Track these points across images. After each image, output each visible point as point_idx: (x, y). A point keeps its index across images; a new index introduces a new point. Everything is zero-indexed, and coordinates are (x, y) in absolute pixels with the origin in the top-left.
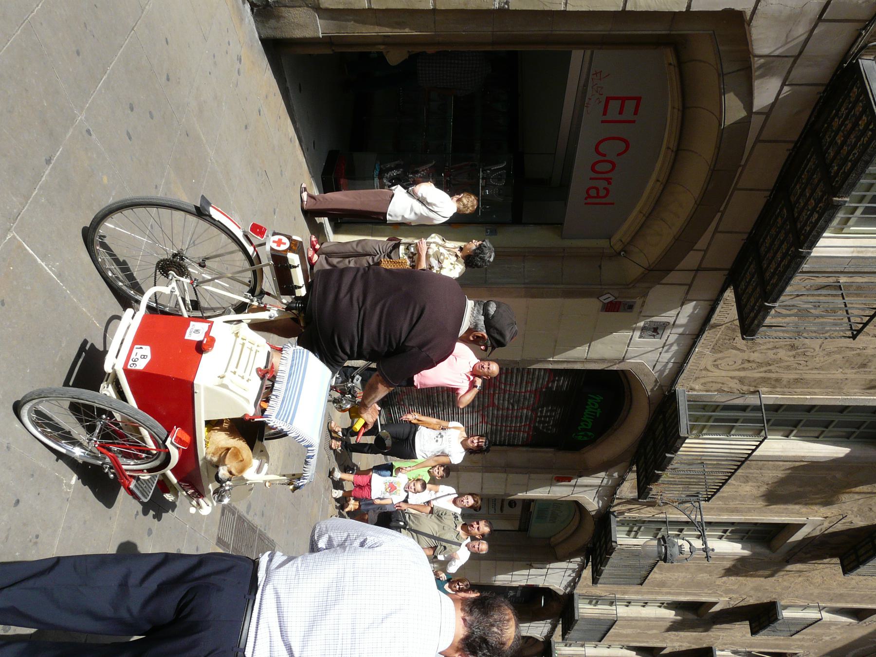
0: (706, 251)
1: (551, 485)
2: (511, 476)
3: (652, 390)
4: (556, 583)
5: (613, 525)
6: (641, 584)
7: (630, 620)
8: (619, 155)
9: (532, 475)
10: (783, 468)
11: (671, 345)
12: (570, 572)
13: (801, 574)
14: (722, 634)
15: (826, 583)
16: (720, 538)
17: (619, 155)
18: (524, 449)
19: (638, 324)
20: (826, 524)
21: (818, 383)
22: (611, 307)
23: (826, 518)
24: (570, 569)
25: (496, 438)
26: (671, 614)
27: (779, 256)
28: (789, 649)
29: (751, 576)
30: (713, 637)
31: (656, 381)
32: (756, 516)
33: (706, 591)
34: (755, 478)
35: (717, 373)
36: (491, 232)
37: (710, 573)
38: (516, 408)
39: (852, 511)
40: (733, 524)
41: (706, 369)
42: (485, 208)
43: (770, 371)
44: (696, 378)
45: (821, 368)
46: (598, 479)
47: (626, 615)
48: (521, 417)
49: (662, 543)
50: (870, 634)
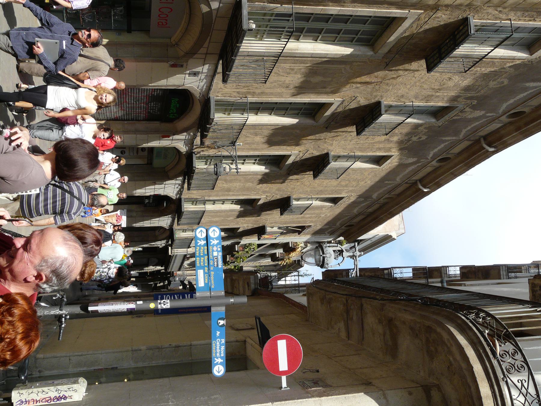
0: (208, 48)
1: (160, 140)
2: (138, 136)
3: (199, 97)
4: (170, 193)
5: (194, 159)
6: (213, 189)
7: (216, 212)
8: (169, 12)
10: (271, 129)
11: (203, 80)
12: (177, 185)
13: (298, 180)
14: (269, 217)
15: (311, 184)
16: (254, 163)
17: (169, 12)
18: (144, 122)
19: (187, 72)
20: (301, 155)
21: (272, 94)
22: (173, 66)
23: (300, 151)
24: (177, 184)
25: (129, 117)
26: (238, 207)
28: (306, 223)
29: (274, 183)
30: (264, 220)
31: (200, 93)
32: (266, 152)
33: (253, 192)
34: (260, 133)
35: (226, 90)
36: (118, 34)
37: (252, 182)
38: (137, 103)
39: (311, 148)
40: (258, 156)
41: (221, 88)
42: (115, 26)
43: (249, 89)
45: (270, 88)
46: (183, 136)
47: (213, 209)
48: (141, 107)
49: (215, 166)
50: (343, 211)
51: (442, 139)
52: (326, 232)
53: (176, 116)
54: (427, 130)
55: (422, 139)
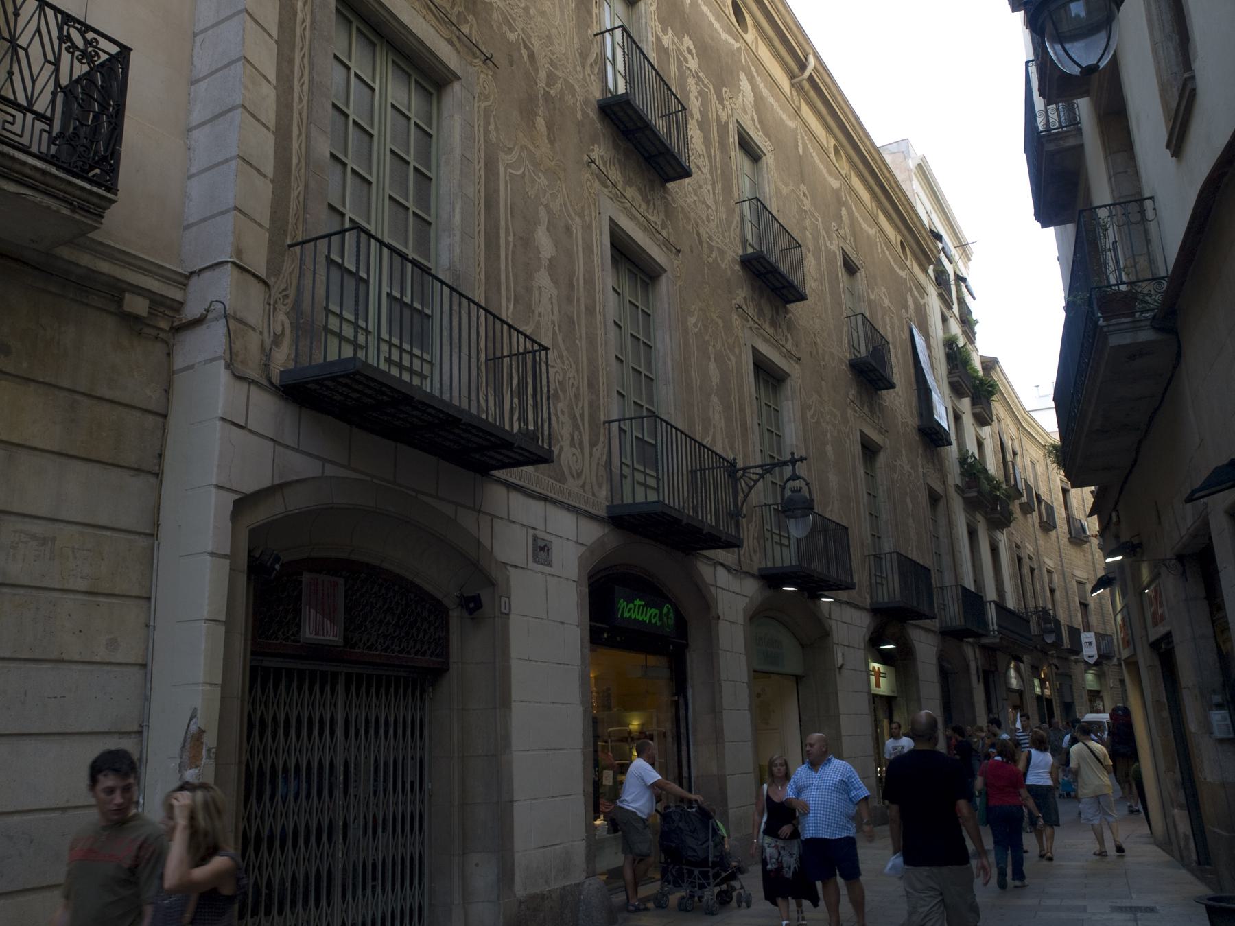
9: (722, 678)
27: (466, 435)
41: (583, 486)
44: (594, 495)
51: (690, 4)
52: (922, 302)
53: (669, 609)
54: (670, 31)
55: (692, 47)
